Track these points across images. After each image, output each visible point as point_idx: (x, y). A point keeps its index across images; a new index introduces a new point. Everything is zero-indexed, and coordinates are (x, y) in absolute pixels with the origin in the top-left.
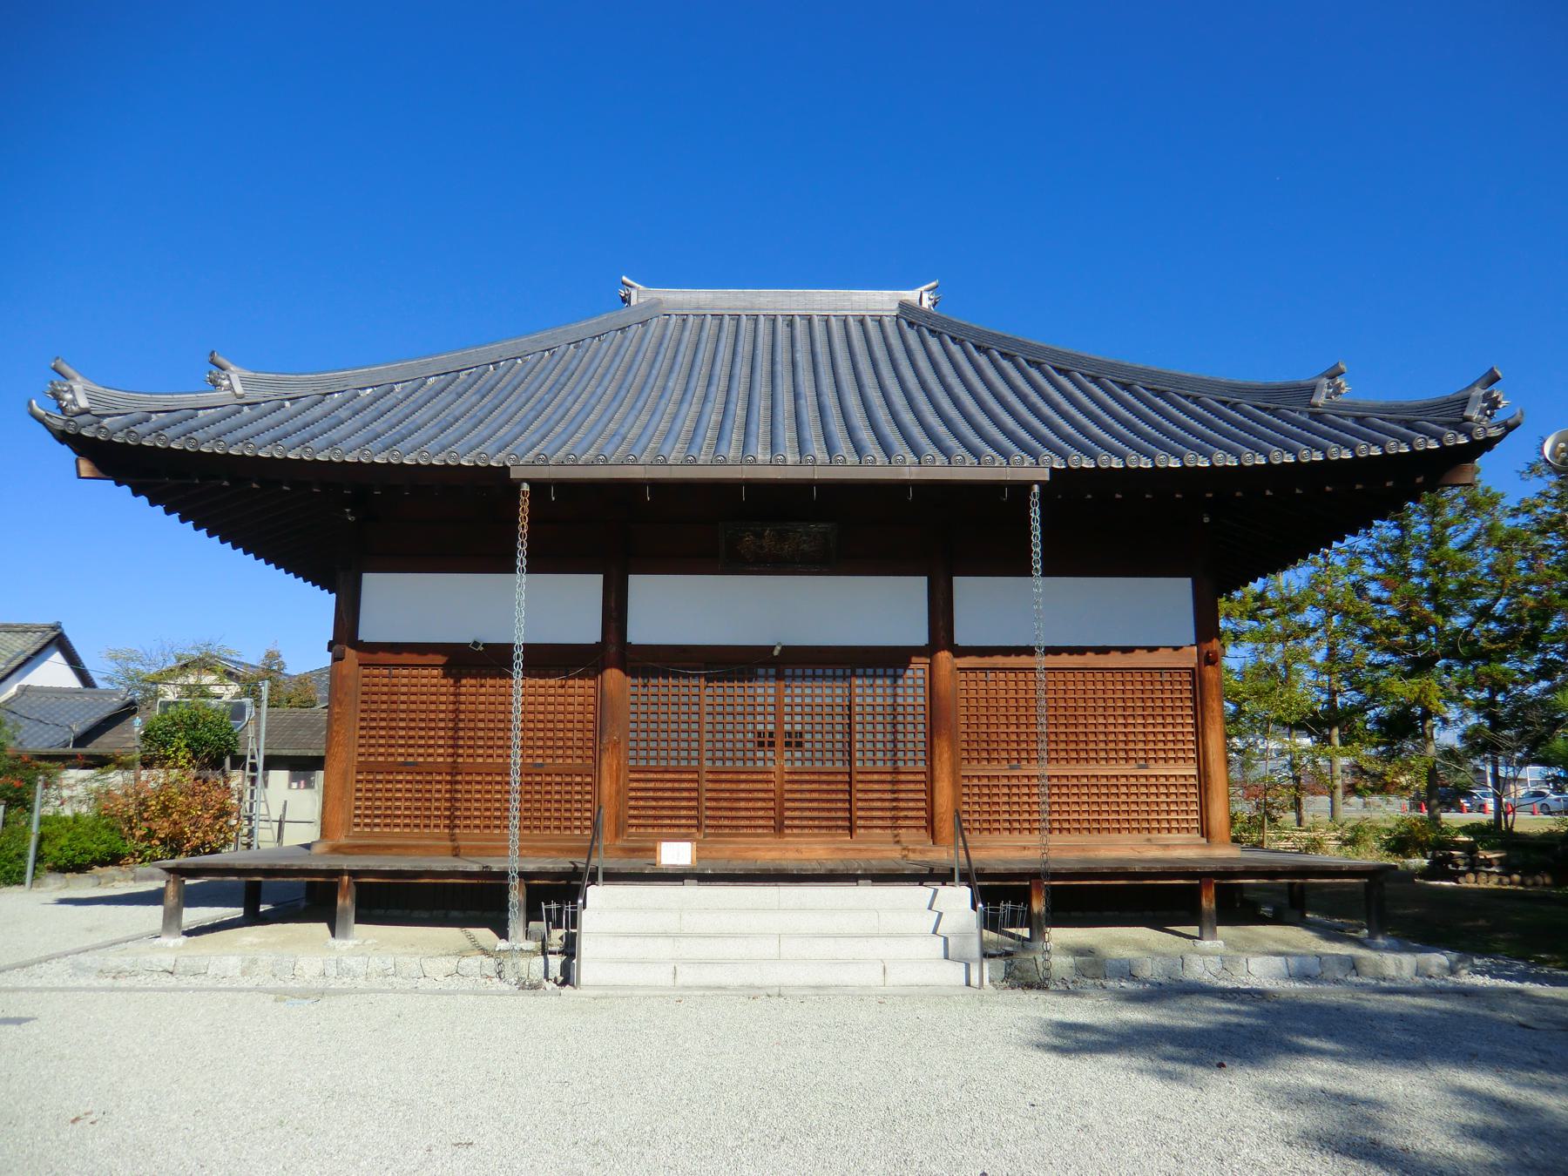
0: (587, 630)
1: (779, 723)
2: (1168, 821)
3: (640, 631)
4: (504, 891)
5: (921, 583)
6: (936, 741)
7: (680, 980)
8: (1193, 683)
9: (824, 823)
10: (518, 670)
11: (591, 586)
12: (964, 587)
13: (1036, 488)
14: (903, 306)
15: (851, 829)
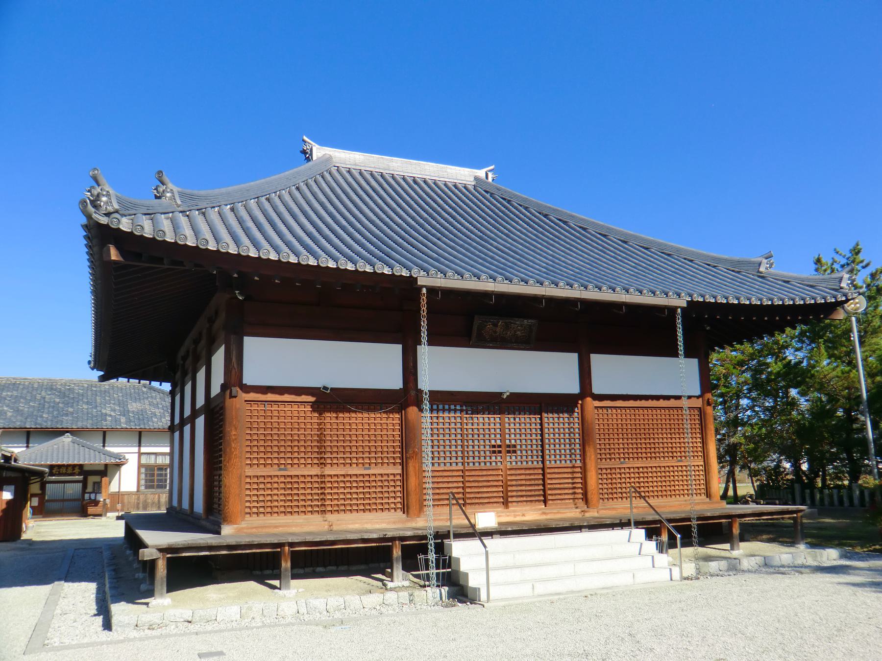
0: (395, 382)
1: (503, 440)
2: (351, 505)
3: (426, 382)
4: (389, 550)
5: (575, 356)
6: (587, 448)
7: (536, 593)
8: (700, 415)
9: (529, 499)
10: (426, 405)
11: (572, 359)
12: (426, 353)
13: (679, 310)
14: (476, 179)
15: (507, 507)
